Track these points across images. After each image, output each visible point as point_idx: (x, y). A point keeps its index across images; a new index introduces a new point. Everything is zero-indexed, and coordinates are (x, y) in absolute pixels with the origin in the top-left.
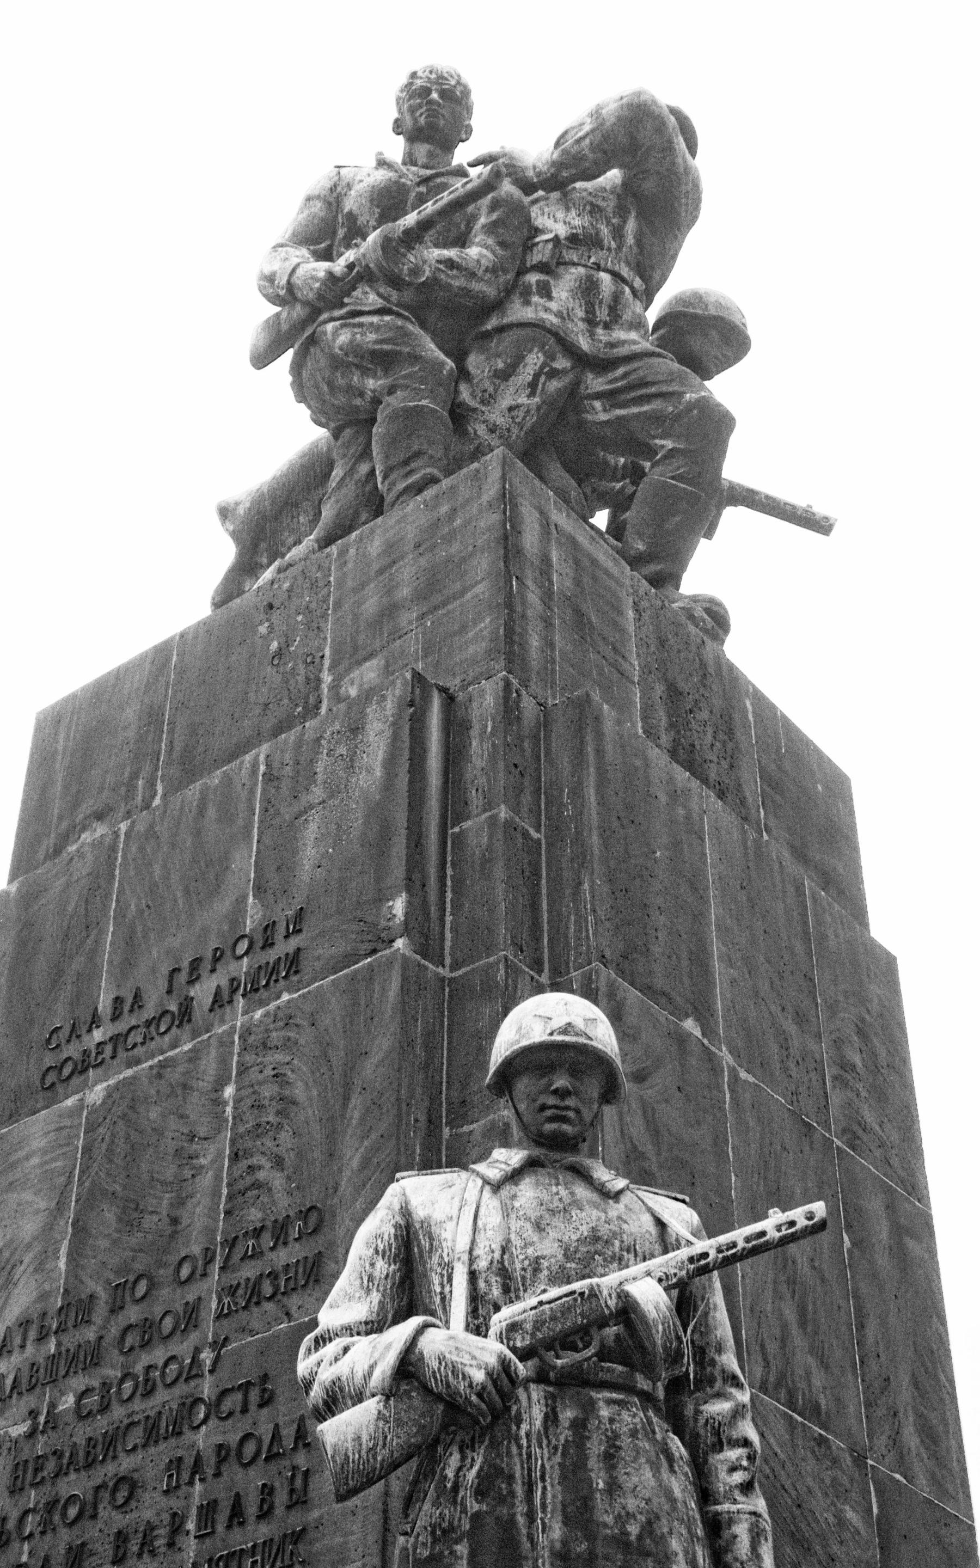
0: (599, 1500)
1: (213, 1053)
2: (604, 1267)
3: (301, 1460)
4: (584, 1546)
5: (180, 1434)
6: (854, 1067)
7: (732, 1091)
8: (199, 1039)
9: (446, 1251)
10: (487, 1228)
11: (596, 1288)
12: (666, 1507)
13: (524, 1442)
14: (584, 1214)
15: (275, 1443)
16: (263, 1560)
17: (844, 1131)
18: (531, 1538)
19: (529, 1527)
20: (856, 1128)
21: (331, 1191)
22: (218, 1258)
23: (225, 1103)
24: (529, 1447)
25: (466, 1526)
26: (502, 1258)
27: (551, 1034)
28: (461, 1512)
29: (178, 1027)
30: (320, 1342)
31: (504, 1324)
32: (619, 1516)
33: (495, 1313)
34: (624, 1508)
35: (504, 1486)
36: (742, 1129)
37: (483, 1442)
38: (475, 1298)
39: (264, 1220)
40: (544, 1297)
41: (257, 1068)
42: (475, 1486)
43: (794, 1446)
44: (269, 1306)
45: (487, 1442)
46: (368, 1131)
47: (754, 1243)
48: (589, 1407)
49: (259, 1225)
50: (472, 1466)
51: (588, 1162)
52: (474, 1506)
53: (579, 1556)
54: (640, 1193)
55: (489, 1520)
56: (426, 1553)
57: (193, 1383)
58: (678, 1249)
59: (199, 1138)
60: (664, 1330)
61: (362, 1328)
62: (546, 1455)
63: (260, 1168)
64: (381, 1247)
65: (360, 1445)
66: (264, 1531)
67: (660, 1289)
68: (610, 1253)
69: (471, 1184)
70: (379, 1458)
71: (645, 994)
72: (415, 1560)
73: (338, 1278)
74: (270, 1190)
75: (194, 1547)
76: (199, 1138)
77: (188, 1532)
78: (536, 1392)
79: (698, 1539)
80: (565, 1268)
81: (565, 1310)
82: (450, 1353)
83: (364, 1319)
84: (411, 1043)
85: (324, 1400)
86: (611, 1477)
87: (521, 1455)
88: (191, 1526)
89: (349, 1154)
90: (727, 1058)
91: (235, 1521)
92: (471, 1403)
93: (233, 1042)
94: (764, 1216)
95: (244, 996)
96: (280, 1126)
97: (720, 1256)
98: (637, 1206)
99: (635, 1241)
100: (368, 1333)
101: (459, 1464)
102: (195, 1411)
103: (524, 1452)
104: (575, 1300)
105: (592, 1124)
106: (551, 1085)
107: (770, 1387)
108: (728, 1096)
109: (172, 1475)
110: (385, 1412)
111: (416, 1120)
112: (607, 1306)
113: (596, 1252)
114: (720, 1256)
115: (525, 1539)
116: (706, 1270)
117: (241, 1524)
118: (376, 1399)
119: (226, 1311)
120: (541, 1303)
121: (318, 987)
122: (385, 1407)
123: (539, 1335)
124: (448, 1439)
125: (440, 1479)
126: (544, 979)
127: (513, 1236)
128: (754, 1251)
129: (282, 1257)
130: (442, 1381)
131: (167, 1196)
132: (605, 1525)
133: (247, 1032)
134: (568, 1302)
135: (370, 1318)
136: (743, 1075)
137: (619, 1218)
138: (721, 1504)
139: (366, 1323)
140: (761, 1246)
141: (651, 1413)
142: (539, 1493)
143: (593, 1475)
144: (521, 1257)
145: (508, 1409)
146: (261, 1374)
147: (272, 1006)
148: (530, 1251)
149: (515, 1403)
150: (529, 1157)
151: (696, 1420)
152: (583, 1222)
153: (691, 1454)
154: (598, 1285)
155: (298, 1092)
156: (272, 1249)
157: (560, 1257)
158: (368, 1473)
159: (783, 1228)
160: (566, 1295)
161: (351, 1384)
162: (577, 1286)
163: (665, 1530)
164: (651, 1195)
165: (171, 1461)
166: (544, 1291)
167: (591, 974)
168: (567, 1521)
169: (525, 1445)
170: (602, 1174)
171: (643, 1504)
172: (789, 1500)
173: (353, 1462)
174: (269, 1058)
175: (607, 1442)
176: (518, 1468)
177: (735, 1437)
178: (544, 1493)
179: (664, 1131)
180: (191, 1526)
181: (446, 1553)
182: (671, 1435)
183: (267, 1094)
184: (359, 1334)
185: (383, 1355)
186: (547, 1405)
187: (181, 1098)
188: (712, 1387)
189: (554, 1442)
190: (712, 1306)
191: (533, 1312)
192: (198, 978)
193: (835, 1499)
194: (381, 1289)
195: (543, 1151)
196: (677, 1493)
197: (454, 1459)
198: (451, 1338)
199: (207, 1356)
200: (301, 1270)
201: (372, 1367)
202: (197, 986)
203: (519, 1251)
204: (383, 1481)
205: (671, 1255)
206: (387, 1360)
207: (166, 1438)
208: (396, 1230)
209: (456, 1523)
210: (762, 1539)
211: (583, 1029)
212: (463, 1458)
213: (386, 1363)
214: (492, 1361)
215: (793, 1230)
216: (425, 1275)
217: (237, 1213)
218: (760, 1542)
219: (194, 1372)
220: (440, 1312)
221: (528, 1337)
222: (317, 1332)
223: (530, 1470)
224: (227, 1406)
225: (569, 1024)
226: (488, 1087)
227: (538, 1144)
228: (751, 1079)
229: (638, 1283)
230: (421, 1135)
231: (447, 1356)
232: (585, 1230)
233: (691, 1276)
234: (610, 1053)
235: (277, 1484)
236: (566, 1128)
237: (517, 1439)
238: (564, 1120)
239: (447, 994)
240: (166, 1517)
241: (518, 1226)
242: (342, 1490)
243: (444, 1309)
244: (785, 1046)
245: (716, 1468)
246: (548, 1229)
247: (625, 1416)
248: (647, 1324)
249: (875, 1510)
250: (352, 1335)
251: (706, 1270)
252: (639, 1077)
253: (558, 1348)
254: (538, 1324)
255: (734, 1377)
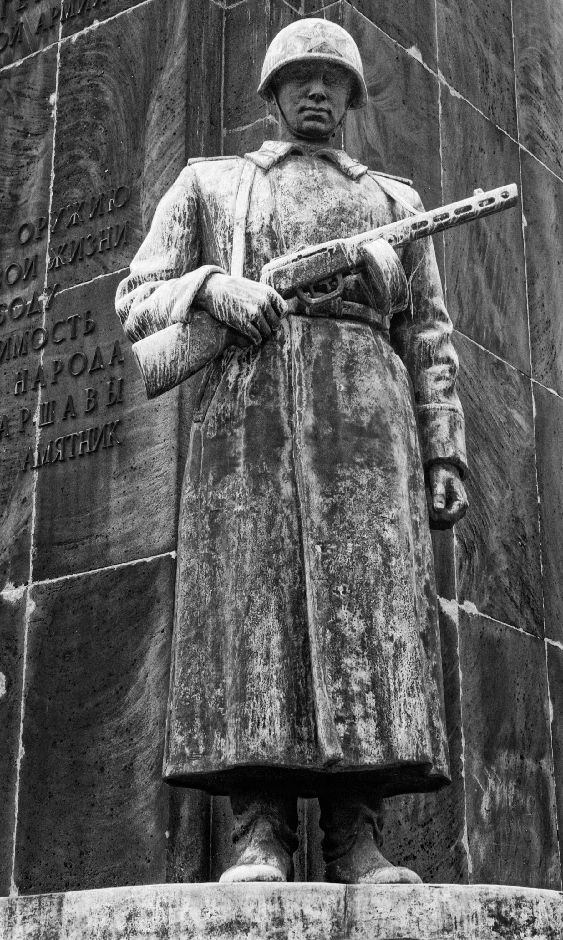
0: (341, 399)
1: (40, 67)
2: (347, 231)
3: (118, 372)
4: (330, 430)
5: (25, 354)
6: (537, 90)
7: (444, 105)
8: (29, 57)
9: (227, 218)
10: (259, 201)
11: (342, 247)
12: (390, 404)
13: (286, 357)
14: (333, 191)
15: (98, 361)
16: (90, 442)
17: (528, 137)
18: (290, 424)
19: (289, 417)
20: (535, 135)
21: (135, 176)
22: (49, 226)
23: (51, 107)
24: (290, 360)
25: (243, 416)
26: (270, 223)
27: (310, 51)
28: (239, 407)
29: (11, 46)
30: (132, 285)
31: (272, 272)
32: (356, 409)
33: (265, 264)
34: (359, 404)
35: (271, 388)
36: (451, 134)
37: (255, 358)
38: (250, 253)
39: (84, 198)
40: (303, 253)
41: (74, 80)
42: (249, 388)
43: (479, 367)
44: (88, 262)
45: (259, 357)
46: (164, 130)
47: (462, 214)
48: (335, 333)
49: (80, 202)
50: (247, 374)
51: (337, 152)
52: (248, 402)
53: (325, 437)
54: (376, 177)
55: (259, 412)
56: (214, 435)
57: (34, 319)
58: (403, 218)
59: (32, 134)
60: (393, 278)
61: (164, 275)
62: (302, 368)
63: (80, 157)
64: (177, 215)
65: (165, 358)
66: (90, 423)
67: (390, 247)
68: (352, 221)
69: (246, 167)
70: (179, 368)
71: (379, 26)
72: (206, 439)
73: (142, 242)
74: (88, 174)
75: (39, 434)
76: (32, 134)
77: (34, 424)
78: (297, 322)
79: (412, 427)
80: (318, 232)
81: (319, 262)
82: (232, 292)
83: (165, 269)
84: (196, 62)
85: (136, 327)
86: (350, 382)
87: (284, 366)
88: (36, 419)
89: (150, 146)
90: (441, 79)
91: (69, 415)
92: (247, 328)
93: (56, 59)
94: (470, 194)
95: (63, 22)
96: (94, 126)
97: (436, 223)
98: (373, 186)
99: (371, 212)
100: (168, 279)
101: (238, 373)
102: (36, 338)
103: (286, 364)
104: (326, 255)
105: (340, 123)
106: (308, 91)
107: (463, 325)
108: (440, 108)
109: (21, 383)
110: (183, 334)
111: (201, 122)
112: (350, 259)
113: (342, 220)
114: (436, 223)
115: (287, 425)
116: (424, 234)
117: (74, 418)
118: (176, 325)
119: (57, 265)
120: (300, 257)
121: (122, 16)
122: (183, 331)
123: (299, 280)
124: (230, 355)
125: (223, 384)
126: (301, 12)
127: (279, 208)
128: (462, 220)
129: (100, 225)
130: (225, 312)
131: (8, 179)
132: (345, 416)
133: (66, 50)
134: (320, 256)
135: (170, 268)
136: (453, 92)
137: (360, 195)
138: (428, 403)
139: (167, 271)
140: (467, 216)
141: (380, 338)
142: (297, 393)
143: (337, 381)
144: (285, 223)
145: (274, 333)
146: (85, 312)
147: (85, 31)
148: (292, 218)
149: (280, 329)
150: (291, 148)
151: (412, 345)
152: (333, 197)
153: (408, 369)
154: (343, 244)
155: (109, 99)
156: (91, 219)
157: (315, 223)
158: (171, 378)
159: (485, 203)
160: (319, 251)
161: (157, 315)
162: (329, 244)
163: (389, 420)
164: (384, 178)
165: (19, 374)
166: (303, 248)
167: (338, 9)
168: (317, 414)
169: (287, 359)
170: (346, 161)
171: (373, 402)
172: (474, 406)
173: (160, 370)
174: (83, 73)
175: (348, 358)
176: (282, 376)
177: (440, 356)
178: (301, 394)
179: (391, 135)
180: (36, 419)
181: (229, 434)
182: (394, 354)
183: (84, 101)
184: (161, 279)
185: (181, 293)
186: (303, 331)
187: (15, 102)
188: (425, 321)
189: (308, 358)
190: (427, 262)
191: (294, 263)
192: (25, 8)
193: (506, 405)
194: (178, 246)
195: (302, 143)
196: (398, 395)
197: (235, 370)
198: (232, 281)
199: (44, 298)
200: (114, 235)
201: (173, 302)
202: (25, 14)
203: (283, 218)
204: (177, 388)
205: (398, 222)
206: (184, 297)
207: (15, 357)
208: (189, 202)
209: (236, 414)
210: (458, 427)
211: (335, 47)
212: (241, 369)
213: (183, 299)
214: (264, 300)
215: (492, 205)
216: (213, 237)
217: (63, 192)
218: (456, 430)
219: (35, 310)
220: (223, 263)
221: (290, 281)
222: (130, 278)
223: (290, 377)
224: (60, 334)
225: (324, 43)
226: (260, 92)
227: (299, 138)
228: (459, 96)
229: (374, 243)
230: (205, 132)
231: (230, 294)
232: (334, 204)
233: (413, 238)
234: (355, 68)
235: (99, 390)
236: (320, 125)
237: (281, 355)
238: (319, 119)
239: (224, 23)
240: (18, 413)
241: (283, 200)
242: (152, 389)
243: (227, 261)
244: (486, 70)
245: (426, 378)
246: (305, 202)
247: (361, 339)
248: (380, 273)
249: (535, 414)
250: (156, 280)
251: (424, 234)
252: (374, 91)
253: (312, 290)
254: (298, 272)
255: (442, 313)
